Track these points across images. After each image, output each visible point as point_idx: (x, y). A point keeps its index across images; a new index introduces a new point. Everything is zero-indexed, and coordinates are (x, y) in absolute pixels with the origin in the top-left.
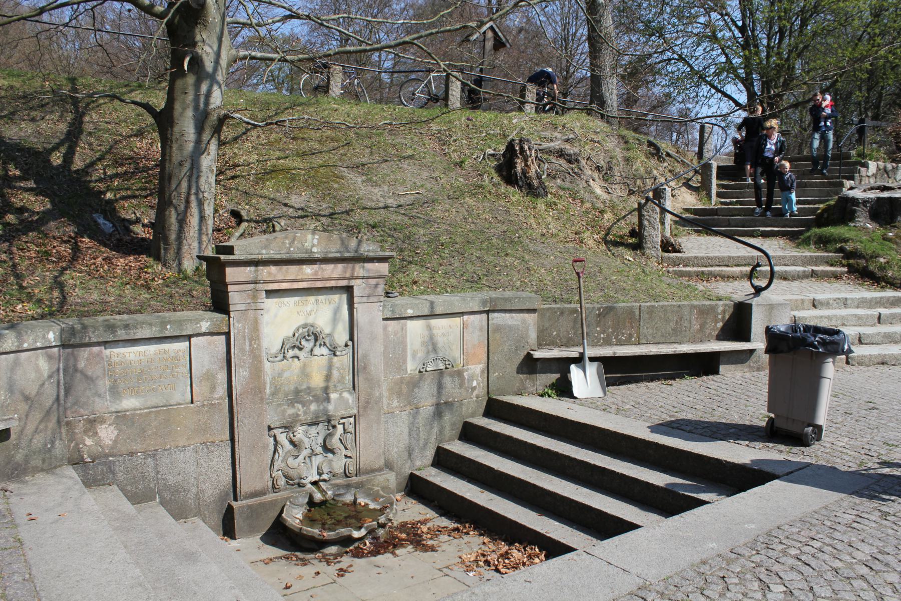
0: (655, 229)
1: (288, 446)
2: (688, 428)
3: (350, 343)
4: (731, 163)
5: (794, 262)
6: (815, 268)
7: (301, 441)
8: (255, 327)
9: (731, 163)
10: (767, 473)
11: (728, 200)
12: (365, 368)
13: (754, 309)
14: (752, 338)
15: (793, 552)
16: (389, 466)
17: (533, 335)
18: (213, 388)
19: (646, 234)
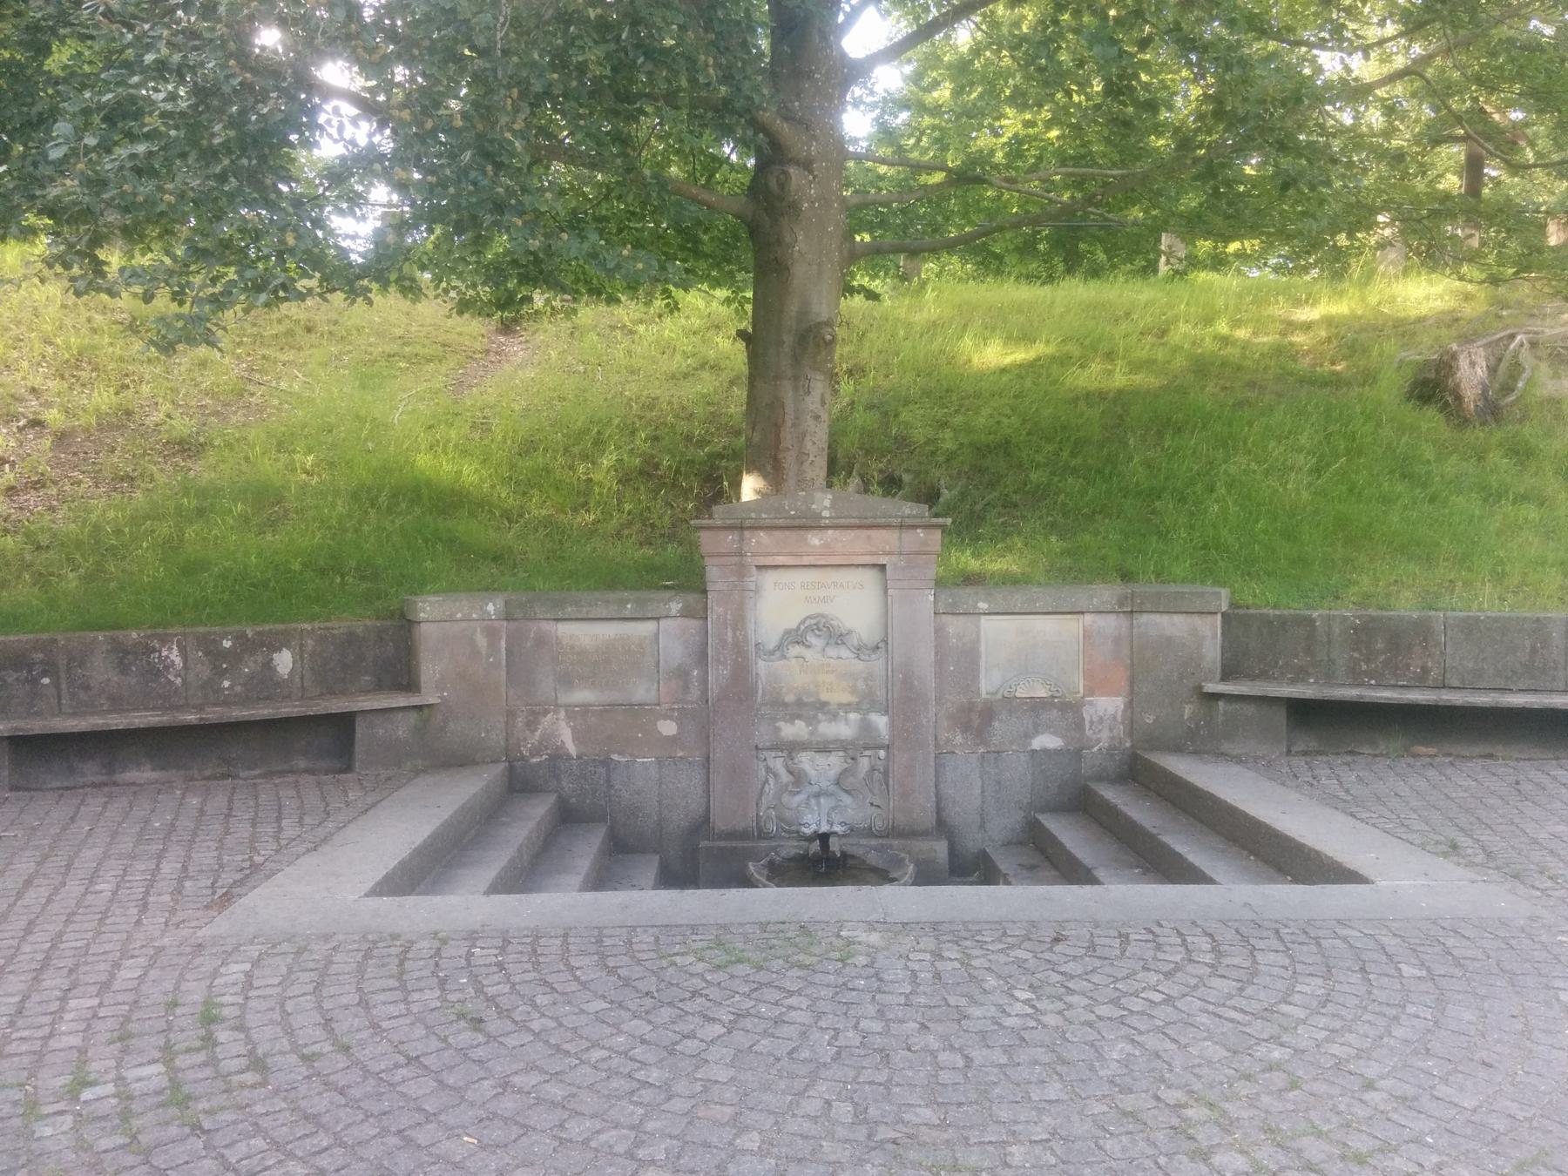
1: (785, 777)
8: (739, 621)
16: (942, 827)
17: (1212, 652)
18: (686, 688)
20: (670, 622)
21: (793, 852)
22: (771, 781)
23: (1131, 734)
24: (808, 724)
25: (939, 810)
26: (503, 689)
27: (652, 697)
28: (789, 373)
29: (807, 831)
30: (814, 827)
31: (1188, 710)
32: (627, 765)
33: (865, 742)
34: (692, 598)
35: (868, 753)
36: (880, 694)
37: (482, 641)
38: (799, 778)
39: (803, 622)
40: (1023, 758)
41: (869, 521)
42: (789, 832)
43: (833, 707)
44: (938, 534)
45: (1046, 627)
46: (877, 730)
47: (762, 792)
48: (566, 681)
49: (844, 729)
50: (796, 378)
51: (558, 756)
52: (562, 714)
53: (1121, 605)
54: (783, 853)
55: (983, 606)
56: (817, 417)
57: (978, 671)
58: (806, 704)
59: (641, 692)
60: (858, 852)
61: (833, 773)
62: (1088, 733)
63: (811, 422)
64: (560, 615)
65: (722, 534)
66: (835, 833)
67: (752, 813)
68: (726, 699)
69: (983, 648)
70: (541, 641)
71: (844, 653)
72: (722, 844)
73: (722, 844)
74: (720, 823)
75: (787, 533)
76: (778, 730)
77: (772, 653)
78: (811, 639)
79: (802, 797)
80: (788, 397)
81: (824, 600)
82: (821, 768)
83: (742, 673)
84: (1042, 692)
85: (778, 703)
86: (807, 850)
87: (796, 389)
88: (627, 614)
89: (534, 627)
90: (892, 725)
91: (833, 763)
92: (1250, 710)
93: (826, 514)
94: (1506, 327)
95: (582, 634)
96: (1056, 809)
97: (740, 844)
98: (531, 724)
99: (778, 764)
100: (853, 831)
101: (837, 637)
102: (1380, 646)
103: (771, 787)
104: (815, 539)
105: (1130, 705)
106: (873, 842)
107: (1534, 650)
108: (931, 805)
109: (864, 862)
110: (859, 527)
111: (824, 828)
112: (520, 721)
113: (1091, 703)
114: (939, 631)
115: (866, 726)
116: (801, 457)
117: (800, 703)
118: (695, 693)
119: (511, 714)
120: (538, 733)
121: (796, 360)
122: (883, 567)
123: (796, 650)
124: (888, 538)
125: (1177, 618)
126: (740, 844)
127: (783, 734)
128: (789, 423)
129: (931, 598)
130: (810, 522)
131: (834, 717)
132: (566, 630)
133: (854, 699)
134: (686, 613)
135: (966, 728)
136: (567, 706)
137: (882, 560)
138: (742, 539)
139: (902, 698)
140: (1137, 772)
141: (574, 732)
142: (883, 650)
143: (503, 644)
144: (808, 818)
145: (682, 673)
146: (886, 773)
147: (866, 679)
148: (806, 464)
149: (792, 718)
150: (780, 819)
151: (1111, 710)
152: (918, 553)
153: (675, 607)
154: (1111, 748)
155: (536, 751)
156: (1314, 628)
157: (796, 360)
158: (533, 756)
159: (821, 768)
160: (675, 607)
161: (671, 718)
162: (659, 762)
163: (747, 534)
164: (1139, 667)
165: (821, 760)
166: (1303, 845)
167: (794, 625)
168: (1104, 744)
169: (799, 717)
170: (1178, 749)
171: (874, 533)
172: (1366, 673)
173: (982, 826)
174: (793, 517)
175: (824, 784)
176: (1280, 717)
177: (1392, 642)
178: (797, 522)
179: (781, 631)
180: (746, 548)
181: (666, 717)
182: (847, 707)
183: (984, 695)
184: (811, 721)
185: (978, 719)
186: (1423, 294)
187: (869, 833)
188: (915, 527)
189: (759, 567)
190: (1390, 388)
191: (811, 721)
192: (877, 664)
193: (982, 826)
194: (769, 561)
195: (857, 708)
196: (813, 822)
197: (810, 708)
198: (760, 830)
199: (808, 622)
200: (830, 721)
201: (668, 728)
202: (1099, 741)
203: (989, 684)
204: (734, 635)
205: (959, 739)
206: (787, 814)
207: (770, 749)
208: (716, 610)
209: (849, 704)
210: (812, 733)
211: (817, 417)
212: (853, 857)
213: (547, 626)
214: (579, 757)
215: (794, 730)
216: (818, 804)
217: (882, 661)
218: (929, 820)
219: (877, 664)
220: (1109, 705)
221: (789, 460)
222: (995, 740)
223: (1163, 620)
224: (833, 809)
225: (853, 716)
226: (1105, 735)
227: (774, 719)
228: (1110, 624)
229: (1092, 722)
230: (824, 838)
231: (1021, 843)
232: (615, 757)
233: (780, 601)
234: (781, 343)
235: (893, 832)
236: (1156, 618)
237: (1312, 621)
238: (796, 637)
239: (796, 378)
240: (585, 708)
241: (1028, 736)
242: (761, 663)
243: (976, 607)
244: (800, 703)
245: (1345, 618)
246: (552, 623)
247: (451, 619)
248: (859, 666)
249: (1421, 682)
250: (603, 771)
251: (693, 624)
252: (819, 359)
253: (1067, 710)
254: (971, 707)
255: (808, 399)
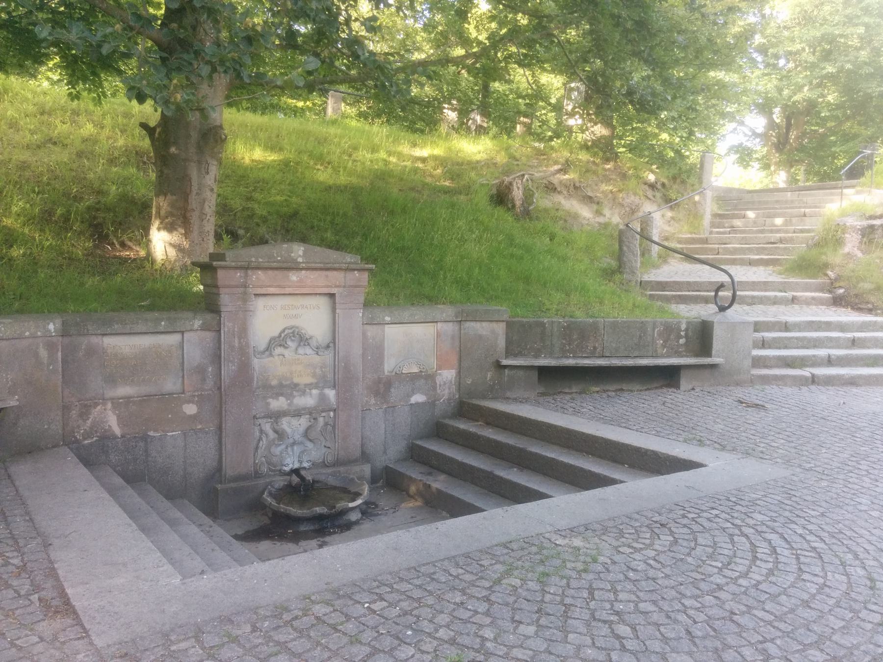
0: (634, 254)
1: (272, 435)
2: (635, 428)
3: (331, 345)
4: (158, 266)
5: (807, 288)
6: (795, 294)
7: (284, 431)
8: (243, 331)
9: (158, 266)
10: (690, 461)
11: (721, 230)
12: (21, 66)
13: (716, 326)
14: (713, 352)
15: (691, 516)
16: (365, 457)
17: (502, 343)
18: (204, 380)
19: (625, 259)
20: (192, 334)
21: (282, 484)
22: (264, 439)
23: (459, 390)
24: (287, 399)
25: (362, 445)
26: (60, 390)
27: (177, 387)
28: (195, 158)
29: (287, 469)
30: (291, 466)
31: (489, 376)
32: (160, 439)
33: (322, 407)
34: (209, 316)
35: (323, 414)
36: (330, 376)
37: (43, 353)
38: (281, 435)
39: (284, 331)
40: (407, 409)
41: (329, 266)
42: (274, 471)
43: (302, 387)
44: (366, 275)
45: (418, 330)
46: (329, 399)
47: (257, 448)
48: (112, 380)
49: (308, 401)
50: (199, 162)
51: (106, 437)
52: (109, 405)
53: (457, 317)
54: (277, 486)
55: (388, 319)
56: (212, 190)
57: (383, 358)
58: (286, 386)
59: (171, 385)
60: (322, 478)
61: (302, 429)
62: (439, 391)
63: (209, 193)
64: (109, 331)
65: (232, 272)
66: (304, 468)
67: (251, 462)
68: (229, 385)
69: (386, 344)
70: (91, 352)
71: (308, 351)
72: (233, 485)
73: (233, 485)
74: (229, 471)
75: (276, 272)
76: (268, 404)
77: (263, 352)
78: (289, 343)
79: (283, 447)
80: (194, 173)
81: (296, 316)
82: (294, 427)
83: (245, 367)
84: (415, 370)
85: (267, 387)
86: (290, 482)
87: (199, 170)
88: (161, 329)
89: (84, 341)
90: (338, 394)
91: (303, 423)
92: (521, 373)
93: (300, 260)
94: (520, 171)
95: (123, 345)
96: (428, 436)
97: (242, 484)
98: (84, 414)
99: (267, 427)
100: (315, 465)
101: (303, 340)
102: (575, 337)
103: (264, 443)
104: (294, 277)
105: (459, 373)
106: (330, 470)
107: (640, 337)
108: (359, 443)
109: (327, 484)
110: (321, 269)
111: (296, 466)
112: (74, 413)
113: (440, 374)
114: (364, 334)
115: (323, 398)
116: (202, 216)
117: (281, 385)
118: (210, 383)
119: (66, 408)
120: (89, 422)
121: (200, 150)
122: (332, 296)
123: (279, 350)
124: (337, 277)
125: (484, 324)
126: (242, 484)
127: (271, 406)
128: (194, 193)
129: (361, 315)
130: (293, 266)
131: (303, 393)
132: (109, 342)
133: (314, 381)
134: (204, 328)
135: (377, 394)
136: (112, 399)
137: (333, 291)
138: (246, 275)
139: (340, 378)
140: (464, 409)
141: (119, 418)
142: (332, 348)
143: (60, 354)
144: (288, 461)
145: (200, 370)
146: (334, 427)
147: (321, 367)
148: (205, 221)
149: (277, 395)
150: (269, 463)
151: (450, 377)
152: (356, 287)
153: (197, 323)
154: (449, 399)
155: (87, 435)
156: (545, 328)
157: (200, 150)
158: (85, 439)
159: (294, 427)
160: (197, 323)
161: (193, 403)
162: (185, 434)
163: (250, 272)
164: (464, 351)
165: (295, 422)
166: (640, 448)
167: (276, 334)
168: (446, 397)
169: (282, 395)
170: (484, 397)
171: (329, 273)
172: (568, 351)
173: (385, 452)
174: (279, 261)
175: (298, 437)
176: (535, 375)
177: (578, 334)
178: (285, 265)
179: (267, 340)
180: (249, 282)
181: (189, 402)
182: (310, 386)
183: (386, 373)
184: (289, 397)
185: (382, 387)
186: (475, 148)
187: (324, 465)
188: (354, 270)
189: (256, 295)
190: (482, 199)
191: (289, 397)
192: (328, 357)
193: (385, 452)
194: (263, 291)
195: (316, 386)
196: (291, 463)
197: (288, 388)
198: (256, 472)
199: (286, 332)
200: (300, 396)
201: (190, 409)
202: (443, 395)
203: (389, 366)
204: (240, 343)
205: (373, 401)
206: (274, 459)
207: (264, 417)
208: (227, 325)
209: (312, 384)
210: (289, 405)
211: (212, 190)
212: (318, 482)
213: (95, 340)
214: (123, 436)
215: (278, 404)
216: (293, 450)
217: (332, 355)
218: (358, 453)
219: (328, 357)
220: (448, 375)
221: (194, 218)
222: (392, 400)
223: (477, 325)
224: (303, 452)
225: (315, 392)
226: (447, 391)
227: (265, 398)
228: (449, 328)
229: (440, 385)
230: (296, 472)
231: (405, 460)
232: (151, 433)
233: (267, 318)
234: (189, 136)
235: (338, 463)
236: (472, 324)
237: (542, 324)
238: (279, 341)
239: (199, 162)
240: (128, 399)
241: (409, 396)
242: (256, 360)
243: (384, 320)
244: (281, 385)
245: (560, 322)
246: (100, 337)
247: (20, 337)
248: (317, 359)
249: (592, 355)
250: (142, 444)
251: (209, 336)
252: (215, 150)
253: (426, 378)
254: (379, 381)
255: (207, 177)
